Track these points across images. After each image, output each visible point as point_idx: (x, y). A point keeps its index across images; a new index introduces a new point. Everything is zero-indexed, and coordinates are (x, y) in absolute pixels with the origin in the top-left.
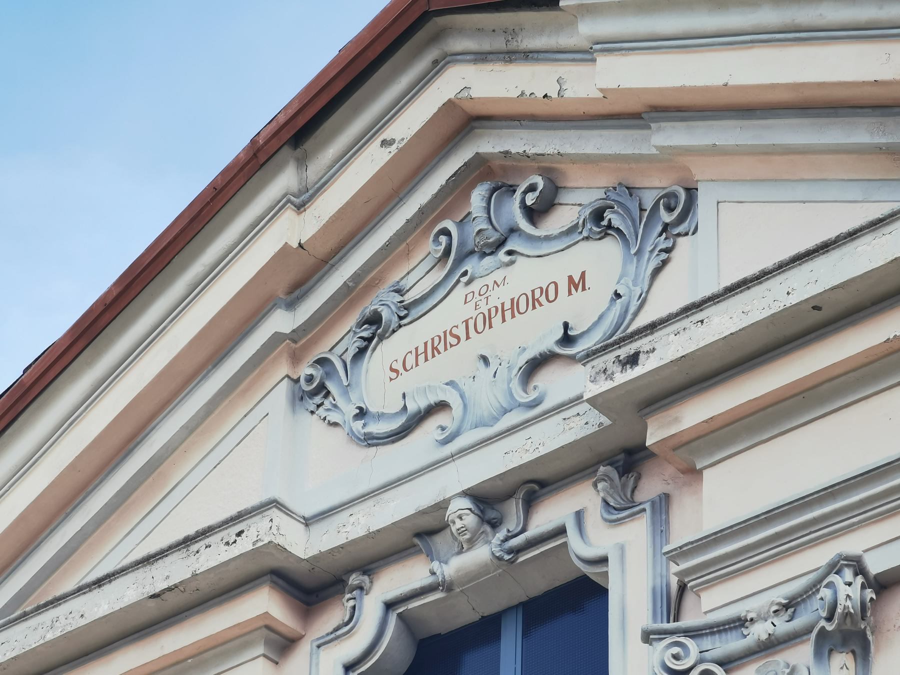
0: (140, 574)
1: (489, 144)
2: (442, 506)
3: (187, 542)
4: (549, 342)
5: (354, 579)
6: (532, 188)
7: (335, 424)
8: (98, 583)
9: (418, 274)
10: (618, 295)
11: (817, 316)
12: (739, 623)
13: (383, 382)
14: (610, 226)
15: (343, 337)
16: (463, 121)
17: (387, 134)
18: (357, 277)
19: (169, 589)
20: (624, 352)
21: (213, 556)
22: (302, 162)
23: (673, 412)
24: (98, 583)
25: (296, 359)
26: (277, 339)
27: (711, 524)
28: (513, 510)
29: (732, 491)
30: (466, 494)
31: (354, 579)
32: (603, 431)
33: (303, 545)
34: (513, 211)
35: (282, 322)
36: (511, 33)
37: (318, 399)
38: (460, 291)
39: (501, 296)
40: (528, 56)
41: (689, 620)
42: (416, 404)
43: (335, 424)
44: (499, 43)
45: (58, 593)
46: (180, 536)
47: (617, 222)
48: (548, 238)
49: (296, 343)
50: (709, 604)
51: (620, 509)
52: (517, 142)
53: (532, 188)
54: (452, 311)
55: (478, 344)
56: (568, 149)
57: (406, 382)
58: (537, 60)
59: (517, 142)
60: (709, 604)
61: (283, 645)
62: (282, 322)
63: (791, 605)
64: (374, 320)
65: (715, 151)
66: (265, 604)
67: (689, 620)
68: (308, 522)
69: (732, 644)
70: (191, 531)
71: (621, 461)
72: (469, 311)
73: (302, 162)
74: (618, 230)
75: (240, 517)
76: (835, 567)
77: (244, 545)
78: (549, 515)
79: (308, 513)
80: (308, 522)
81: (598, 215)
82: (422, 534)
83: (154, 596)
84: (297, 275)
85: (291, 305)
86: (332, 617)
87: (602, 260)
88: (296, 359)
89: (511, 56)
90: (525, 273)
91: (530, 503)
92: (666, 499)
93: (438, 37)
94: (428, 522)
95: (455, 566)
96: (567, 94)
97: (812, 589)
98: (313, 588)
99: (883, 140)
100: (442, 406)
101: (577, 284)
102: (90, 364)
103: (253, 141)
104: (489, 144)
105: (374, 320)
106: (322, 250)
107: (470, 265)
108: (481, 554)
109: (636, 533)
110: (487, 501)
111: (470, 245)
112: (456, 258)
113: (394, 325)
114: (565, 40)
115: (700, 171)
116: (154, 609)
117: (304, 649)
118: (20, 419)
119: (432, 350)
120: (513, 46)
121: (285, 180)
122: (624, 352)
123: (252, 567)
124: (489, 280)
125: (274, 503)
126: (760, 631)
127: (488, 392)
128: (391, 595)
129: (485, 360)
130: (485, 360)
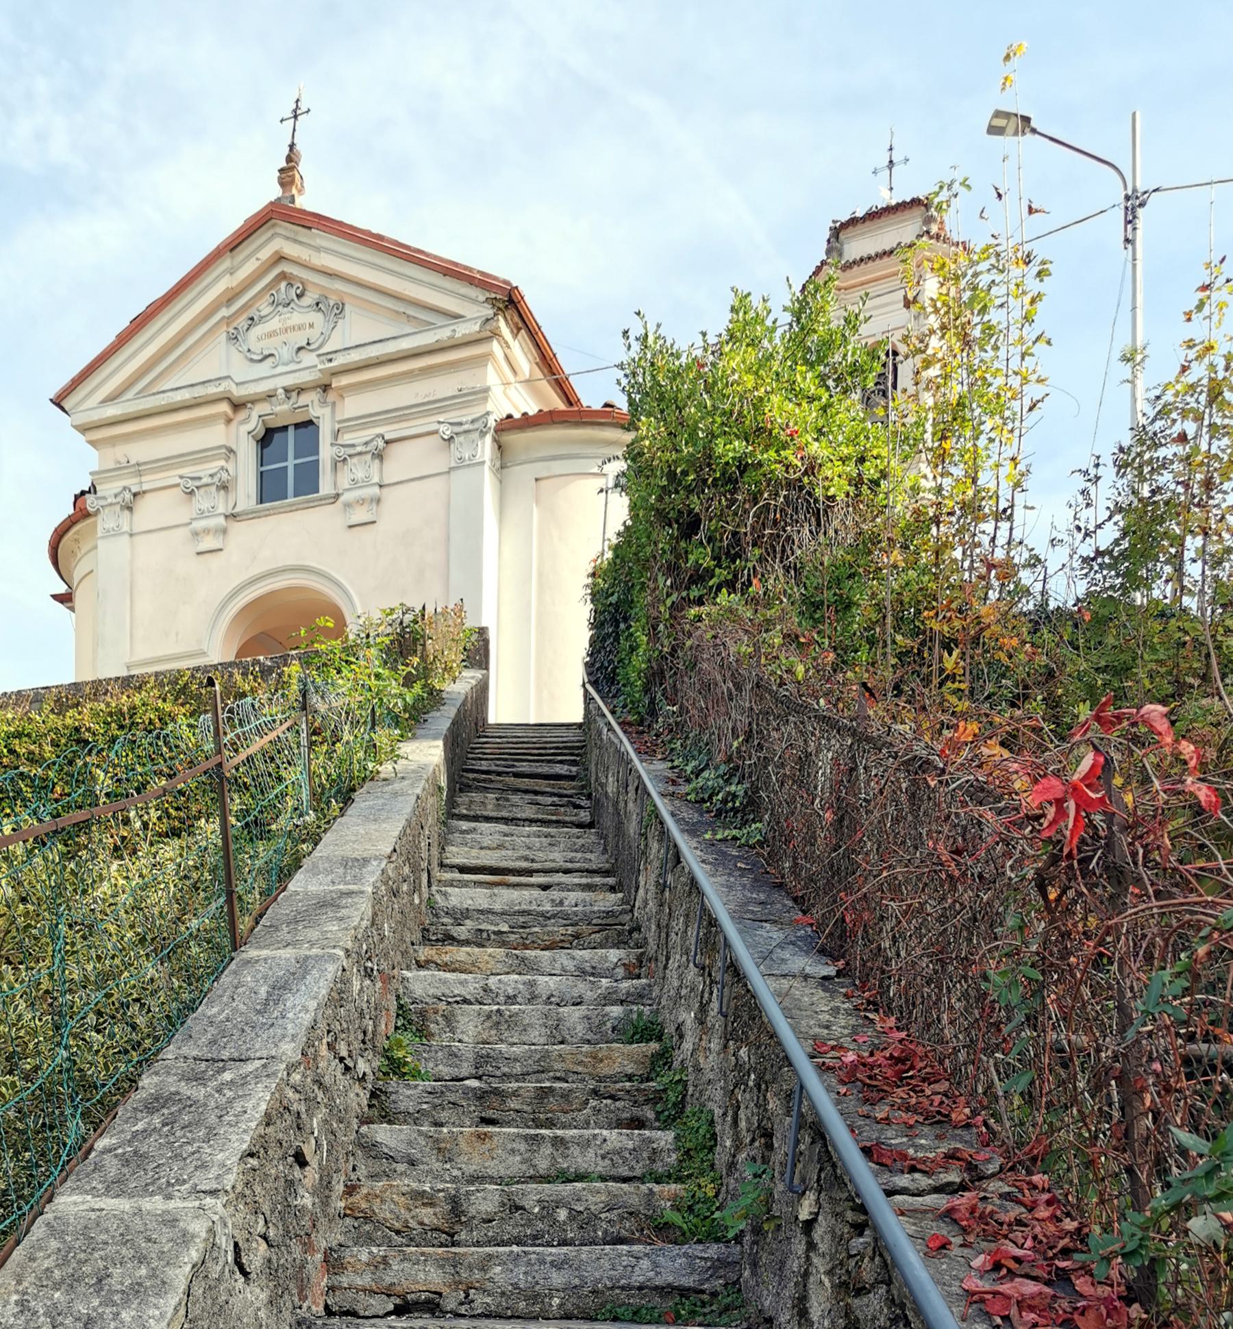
2: (276, 390)
4: (304, 344)
5: (249, 405)
8: (177, 389)
12: (353, 446)
13: (255, 339)
15: (242, 322)
16: (280, 258)
17: (259, 255)
18: (244, 306)
20: (329, 357)
21: (212, 390)
22: (232, 258)
24: (177, 389)
25: (228, 325)
26: (224, 317)
27: (346, 416)
28: (294, 394)
29: (353, 406)
31: (249, 405)
33: (238, 393)
35: (224, 312)
36: (296, 233)
38: (277, 318)
39: (290, 323)
41: (340, 442)
42: (266, 352)
49: (228, 320)
50: (347, 438)
51: (323, 403)
54: (274, 324)
55: (282, 338)
57: (263, 344)
60: (347, 438)
61: (229, 421)
62: (224, 312)
63: (366, 443)
66: (224, 407)
67: (340, 442)
68: (237, 384)
69: (352, 451)
73: (232, 258)
75: (219, 379)
76: (378, 436)
77: (221, 389)
78: (305, 399)
79: (237, 381)
80: (237, 384)
81: (317, 304)
82: (270, 396)
84: (230, 297)
85: (228, 307)
86: (242, 415)
87: (317, 318)
88: (228, 325)
89: (295, 241)
90: (296, 318)
92: (334, 404)
93: (274, 226)
95: (278, 409)
97: (372, 440)
98: (237, 406)
100: (272, 355)
101: (311, 326)
105: (252, 319)
107: (280, 308)
108: (285, 407)
115: (346, 300)
116: (193, 402)
117: (234, 424)
119: (271, 335)
121: (226, 263)
122: (329, 357)
125: (228, 377)
126: (359, 449)
127: (286, 353)
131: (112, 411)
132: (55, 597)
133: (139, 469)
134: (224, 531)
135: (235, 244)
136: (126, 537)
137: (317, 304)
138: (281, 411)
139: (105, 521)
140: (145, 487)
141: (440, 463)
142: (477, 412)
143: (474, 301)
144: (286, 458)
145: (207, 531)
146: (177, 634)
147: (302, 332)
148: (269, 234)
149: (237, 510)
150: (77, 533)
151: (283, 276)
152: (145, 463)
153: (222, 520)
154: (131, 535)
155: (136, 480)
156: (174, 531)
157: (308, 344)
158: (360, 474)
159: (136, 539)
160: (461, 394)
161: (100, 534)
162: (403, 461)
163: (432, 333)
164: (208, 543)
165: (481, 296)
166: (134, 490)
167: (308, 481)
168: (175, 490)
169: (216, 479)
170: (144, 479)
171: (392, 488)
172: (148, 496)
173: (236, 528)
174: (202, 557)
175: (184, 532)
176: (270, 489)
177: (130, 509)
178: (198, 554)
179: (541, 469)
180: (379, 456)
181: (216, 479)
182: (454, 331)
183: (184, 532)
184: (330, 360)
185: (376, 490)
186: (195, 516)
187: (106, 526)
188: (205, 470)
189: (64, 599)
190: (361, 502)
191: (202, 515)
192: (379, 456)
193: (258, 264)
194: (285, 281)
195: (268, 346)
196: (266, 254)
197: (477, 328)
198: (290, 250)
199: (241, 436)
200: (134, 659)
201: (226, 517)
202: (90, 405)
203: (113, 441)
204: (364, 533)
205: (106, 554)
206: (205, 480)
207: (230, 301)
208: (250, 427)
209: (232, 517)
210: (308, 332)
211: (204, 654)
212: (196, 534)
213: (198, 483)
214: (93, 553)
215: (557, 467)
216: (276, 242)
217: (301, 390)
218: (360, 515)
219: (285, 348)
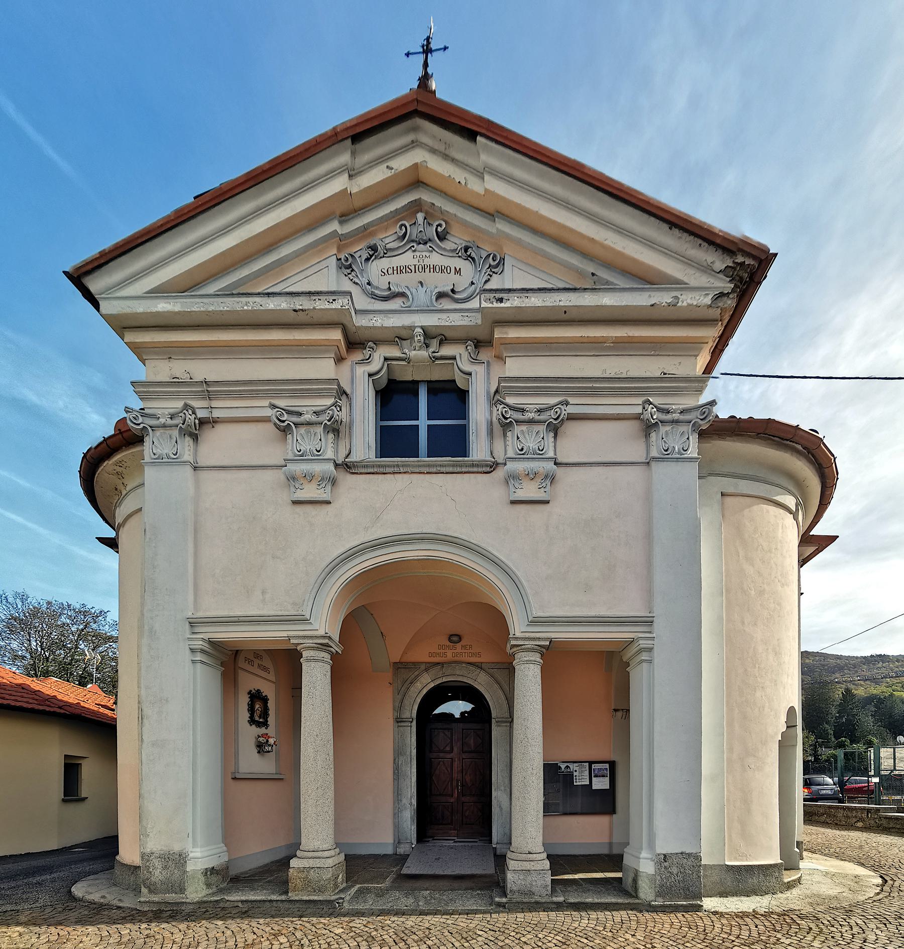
0: (288, 299)
1: (426, 197)
2: (412, 328)
3: (310, 293)
4: (448, 289)
6: (440, 225)
7: (357, 284)
8: (269, 295)
9: (387, 238)
10: (473, 283)
11: (564, 317)
12: (523, 411)
14: (469, 256)
15: (359, 249)
18: (365, 228)
19: (302, 310)
20: (498, 295)
23: (505, 329)
28: (435, 343)
30: (422, 327)
32: (476, 326)
34: (431, 232)
37: (349, 271)
39: (427, 262)
40: (453, 161)
43: (357, 284)
44: (442, 148)
45: (249, 292)
46: (308, 290)
47: (473, 255)
48: (445, 249)
49: (342, 241)
52: (439, 202)
53: (440, 225)
54: (408, 259)
55: (419, 276)
56: (459, 215)
57: (394, 278)
58: (457, 165)
59: (439, 202)
61: (339, 360)
63: (540, 411)
64: (374, 248)
65: (518, 242)
66: (336, 335)
70: (313, 290)
71: (480, 343)
72: (415, 262)
74: (473, 259)
80: (356, 311)
81: (466, 249)
82: (400, 337)
83: (295, 311)
84: (346, 209)
86: (358, 356)
89: (446, 157)
91: (441, 343)
93: (415, 129)
94: (404, 334)
96: (469, 186)
98: (355, 343)
99: (580, 265)
102: (273, 187)
103: (334, 128)
104: (426, 197)
106: (357, 203)
109: (478, 371)
110: (428, 335)
111: (414, 237)
112: (407, 241)
113: (382, 255)
114: (472, 162)
118: (223, 204)
119: (400, 270)
120: (447, 152)
122: (498, 295)
123: (336, 318)
124: (424, 254)
127: (422, 297)
128: (388, 355)
129: (421, 283)
130: (421, 283)
131: (163, 306)
132: (101, 540)
133: (209, 390)
134: (333, 482)
135: (361, 132)
136: (188, 470)
137: (466, 249)
138: (417, 361)
139: (156, 445)
140: (216, 414)
141: (635, 451)
142: (688, 402)
143: (707, 269)
144: (421, 417)
145: (309, 477)
146: (264, 592)
147: (445, 275)
148: (411, 137)
149: (353, 458)
150: (119, 463)
151: (416, 206)
152: (217, 383)
153: (330, 467)
154: (195, 468)
155: (205, 404)
156: (259, 473)
157: (453, 291)
158: (531, 443)
159: (204, 475)
160: (664, 377)
161: (147, 459)
162: (578, 442)
163: (646, 294)
164: (310, 492)
165: (720, 262)
166: (201, 414)
167: (451, 443)
168: (260, 426)
169: (324, 418)
170: (215, 404)
171: (568, 469)
172: (220, 428)
173: (348, 481)
174: (299, 509)
175: (279, 475)
176: (395, 444)
177: (195, 438)
178: (295, 502)
179: (728, 484)
180: (555, 429)
181: (324, 418)
182: (676, 298)
183: (279, 475)
184: (501, 300)
185: (550, 465)
186: (290, 456)
187: (158, 451)
188: (308, 406)
189: (112, 543)
190: (532, 476)
191: (301, 457)
192: (555, 429)
193: (389, 173)
194: (420, 216)
195: (399, 282)
196: (402, 163)
197: (708, 300)
198: (437, 165)
199: (360, 380)
200: (200, 614)
201: (337, 465)
202: (133, 289)
203: (169, 352)
204: (536, 514)
205: (158, 484)
206: (307, 417)
207: (344, 218)
208: (375, 366)
209: (347, 467)
210: (453, 278)
211: (305, 621)
212: (292, 478)
213: (295, 419)
214: (139, 491)
215: (745, 486)
216: (419, 153)
217: (444, 340)
218: (529, 491)
219: (422, 290)
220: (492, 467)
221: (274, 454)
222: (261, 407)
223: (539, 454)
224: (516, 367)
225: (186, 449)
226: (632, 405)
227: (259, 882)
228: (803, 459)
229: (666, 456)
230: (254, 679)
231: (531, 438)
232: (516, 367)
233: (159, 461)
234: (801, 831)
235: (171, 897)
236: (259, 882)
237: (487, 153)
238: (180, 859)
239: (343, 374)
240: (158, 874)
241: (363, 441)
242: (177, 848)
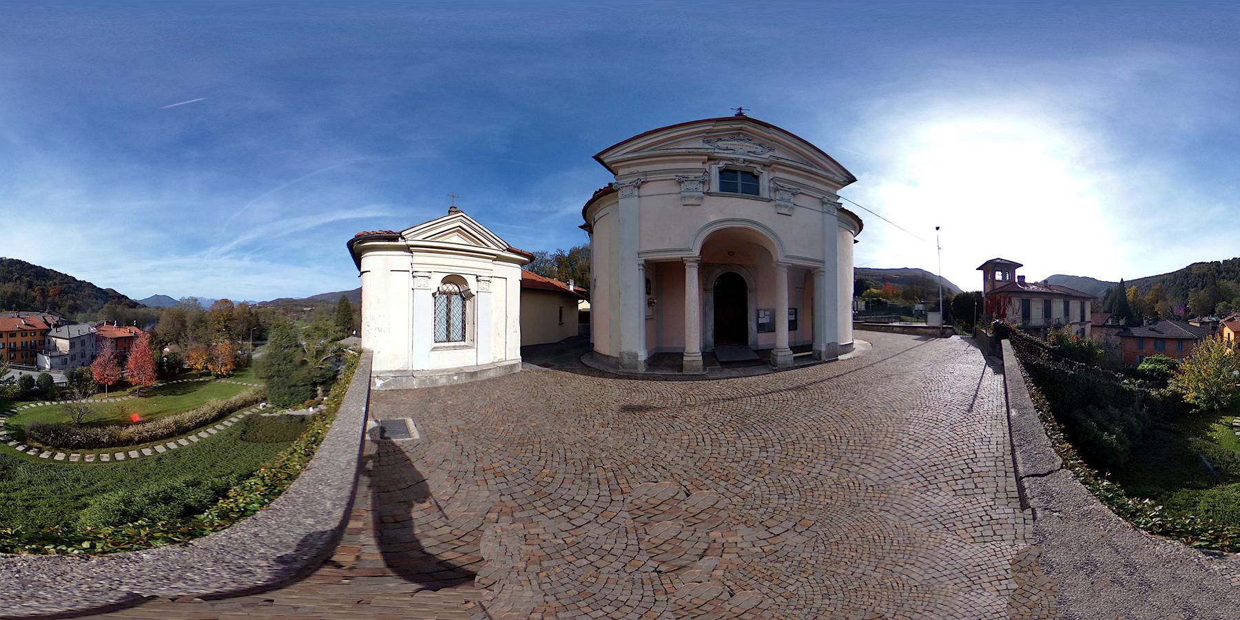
110: (745, 160)
162: (800, 200)
199: (715, 170)
209: (708, 194)
220: (770, 200)
221: (676, 189)
222: (673, 176)
223: (789, 201)
224: (778, 174)
225: (636, 192)
226: (820, 196)
227: (665, 361)
228: (856, 224)
229: (828, 212)
230: (661, 277)
231: (786, 196)
232: (778, 174)
233: (625, 197)
234: (718, 272)
235: (633, 371)
236: (665, 361)
237: (771, 130)
238: (636, 356)
239: (707, 166)
240: (626, 361)
241: (715, 186)
242: (634, 350)
